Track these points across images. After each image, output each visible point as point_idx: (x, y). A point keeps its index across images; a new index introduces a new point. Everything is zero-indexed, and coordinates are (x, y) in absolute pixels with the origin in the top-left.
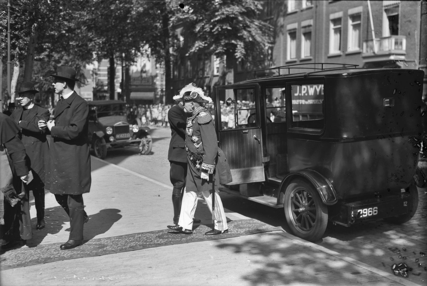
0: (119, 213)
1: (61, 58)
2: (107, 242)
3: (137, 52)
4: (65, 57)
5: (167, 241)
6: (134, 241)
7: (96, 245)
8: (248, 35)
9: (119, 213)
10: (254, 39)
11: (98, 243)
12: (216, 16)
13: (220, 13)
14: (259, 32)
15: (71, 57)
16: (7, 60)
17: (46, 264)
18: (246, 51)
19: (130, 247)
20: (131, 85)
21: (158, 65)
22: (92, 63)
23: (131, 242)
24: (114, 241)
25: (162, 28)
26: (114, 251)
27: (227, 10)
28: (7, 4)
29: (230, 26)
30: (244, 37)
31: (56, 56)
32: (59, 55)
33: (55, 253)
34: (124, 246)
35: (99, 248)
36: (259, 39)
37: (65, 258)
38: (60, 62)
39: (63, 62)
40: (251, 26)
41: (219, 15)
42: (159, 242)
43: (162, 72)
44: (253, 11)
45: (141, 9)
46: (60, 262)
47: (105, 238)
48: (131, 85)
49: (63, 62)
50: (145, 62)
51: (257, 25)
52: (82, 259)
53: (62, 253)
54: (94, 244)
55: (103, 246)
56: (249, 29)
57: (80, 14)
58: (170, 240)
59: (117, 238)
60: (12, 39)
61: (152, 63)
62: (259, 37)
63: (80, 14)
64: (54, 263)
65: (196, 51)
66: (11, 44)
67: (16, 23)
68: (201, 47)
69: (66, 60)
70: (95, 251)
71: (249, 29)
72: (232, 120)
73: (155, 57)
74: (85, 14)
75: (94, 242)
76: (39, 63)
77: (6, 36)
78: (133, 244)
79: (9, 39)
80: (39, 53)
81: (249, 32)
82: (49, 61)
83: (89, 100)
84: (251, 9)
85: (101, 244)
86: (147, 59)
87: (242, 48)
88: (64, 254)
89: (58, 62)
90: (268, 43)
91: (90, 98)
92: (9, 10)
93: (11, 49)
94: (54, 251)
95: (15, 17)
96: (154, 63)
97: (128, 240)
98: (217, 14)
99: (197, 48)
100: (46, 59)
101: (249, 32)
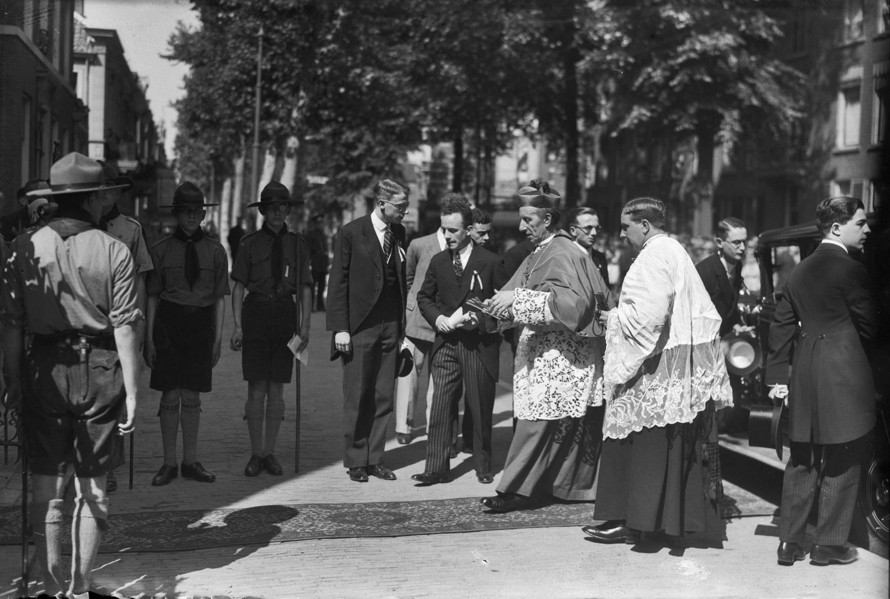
0: (632, 546)
1: (359, 139)
2: (412, 510)
3: (511, 129)
4: (368, 137)
5: (536, 520)
6: (466, 513)
7: (389, 514)
8: (749, 91)
9: (632, 546)
10: (764, 101)
11: (393, 511)
12: (678, 55)
13: (687, 46)
14: (776, 87)
15: (379, 137)
16: (253, 142)
17: (287, 545)
18: (743, 127)
19: (458, 525)
20: (495, 197)
21: (552, 157)
22: (419, 150)
23: (461, 514)
24: (425, 510)
25: (564, 78)
26: (425, 530)
27: (705, 42)
28: (257, 31)
29: (710, 75)
30: (741, 96)
31: (349, 136)
32: (354, 134)
33: (305, 524)
34: (447, 521)
35: (395, 521)
36: (772, 99)
37: (324, 535)
38: (356, 148)
39: (361, 148)
40: (756, 75)
41: (684, 52)
42: (520, 520)
43: (560, 172)
44: (766, 40)
45: (523, 39)
46: (314, 543)
47: (408, 502)
48: (495, 197)
49: (361, 148)
50: (525, 150)
51: (769, 73)
52: (359, 540)
53: (320, 525)
54: (385, 513)
55: (404, 518)
56: (751, 81)
57: (399, 51)
58: (544, 516)
59: (432, 505)
60: (263, 100)
61: (541, 151)
62: (775, 96)
63: (399, 51)
64: (300, 544)
65: (632, 127)
66: (261, 109)
67: (274, 69)
68: (644, 118)
69: (368, 143)
70: (385, 527)
71: (751, 81)
72: (755, 277)
73: (548, 139)
74: (409, 49)
75: (385, 508)
76: (317, 148)
77: (253, 94)
78: (464, 519)
79: (258, 99)
80: (316, 130)
81: (752, 86)
82: (334, 145)
83: (411, 225)
84: (760, 37)
85: (399, 514)
86: (530, 144)
87: (735, 120)
88: (322, 527)
89: (351, 146)
90: (794, 109)
91: (413, 222)
92: (261, 43)
93: (261, 119)
94: (305, 519)
95: (272, 58)
96: (544, 152)
97: (455, 511)
98: (680, 49)
99: (635, 121)
100: (330, 142)
101: (752, 86)
